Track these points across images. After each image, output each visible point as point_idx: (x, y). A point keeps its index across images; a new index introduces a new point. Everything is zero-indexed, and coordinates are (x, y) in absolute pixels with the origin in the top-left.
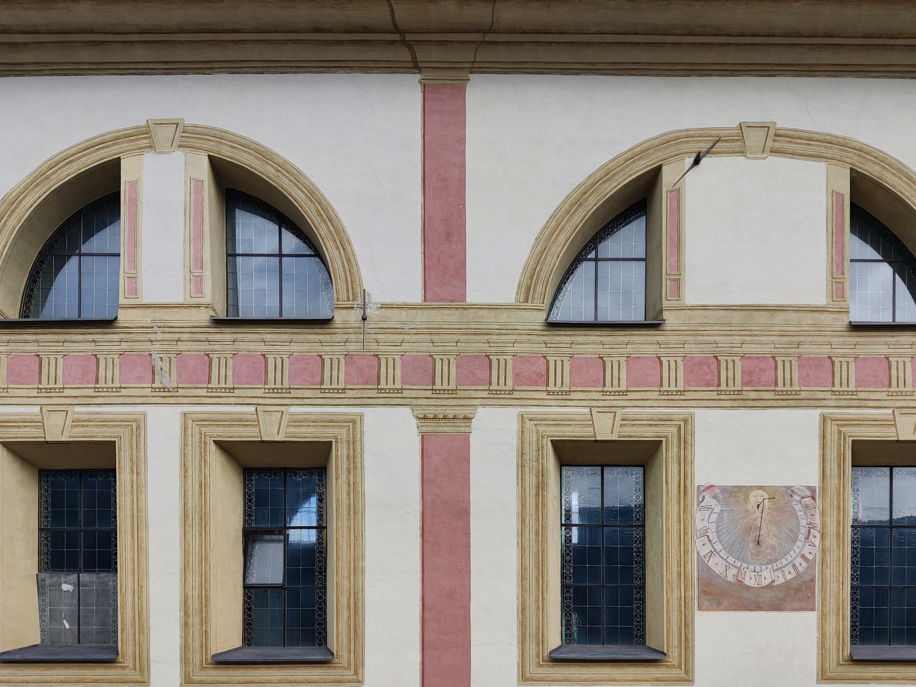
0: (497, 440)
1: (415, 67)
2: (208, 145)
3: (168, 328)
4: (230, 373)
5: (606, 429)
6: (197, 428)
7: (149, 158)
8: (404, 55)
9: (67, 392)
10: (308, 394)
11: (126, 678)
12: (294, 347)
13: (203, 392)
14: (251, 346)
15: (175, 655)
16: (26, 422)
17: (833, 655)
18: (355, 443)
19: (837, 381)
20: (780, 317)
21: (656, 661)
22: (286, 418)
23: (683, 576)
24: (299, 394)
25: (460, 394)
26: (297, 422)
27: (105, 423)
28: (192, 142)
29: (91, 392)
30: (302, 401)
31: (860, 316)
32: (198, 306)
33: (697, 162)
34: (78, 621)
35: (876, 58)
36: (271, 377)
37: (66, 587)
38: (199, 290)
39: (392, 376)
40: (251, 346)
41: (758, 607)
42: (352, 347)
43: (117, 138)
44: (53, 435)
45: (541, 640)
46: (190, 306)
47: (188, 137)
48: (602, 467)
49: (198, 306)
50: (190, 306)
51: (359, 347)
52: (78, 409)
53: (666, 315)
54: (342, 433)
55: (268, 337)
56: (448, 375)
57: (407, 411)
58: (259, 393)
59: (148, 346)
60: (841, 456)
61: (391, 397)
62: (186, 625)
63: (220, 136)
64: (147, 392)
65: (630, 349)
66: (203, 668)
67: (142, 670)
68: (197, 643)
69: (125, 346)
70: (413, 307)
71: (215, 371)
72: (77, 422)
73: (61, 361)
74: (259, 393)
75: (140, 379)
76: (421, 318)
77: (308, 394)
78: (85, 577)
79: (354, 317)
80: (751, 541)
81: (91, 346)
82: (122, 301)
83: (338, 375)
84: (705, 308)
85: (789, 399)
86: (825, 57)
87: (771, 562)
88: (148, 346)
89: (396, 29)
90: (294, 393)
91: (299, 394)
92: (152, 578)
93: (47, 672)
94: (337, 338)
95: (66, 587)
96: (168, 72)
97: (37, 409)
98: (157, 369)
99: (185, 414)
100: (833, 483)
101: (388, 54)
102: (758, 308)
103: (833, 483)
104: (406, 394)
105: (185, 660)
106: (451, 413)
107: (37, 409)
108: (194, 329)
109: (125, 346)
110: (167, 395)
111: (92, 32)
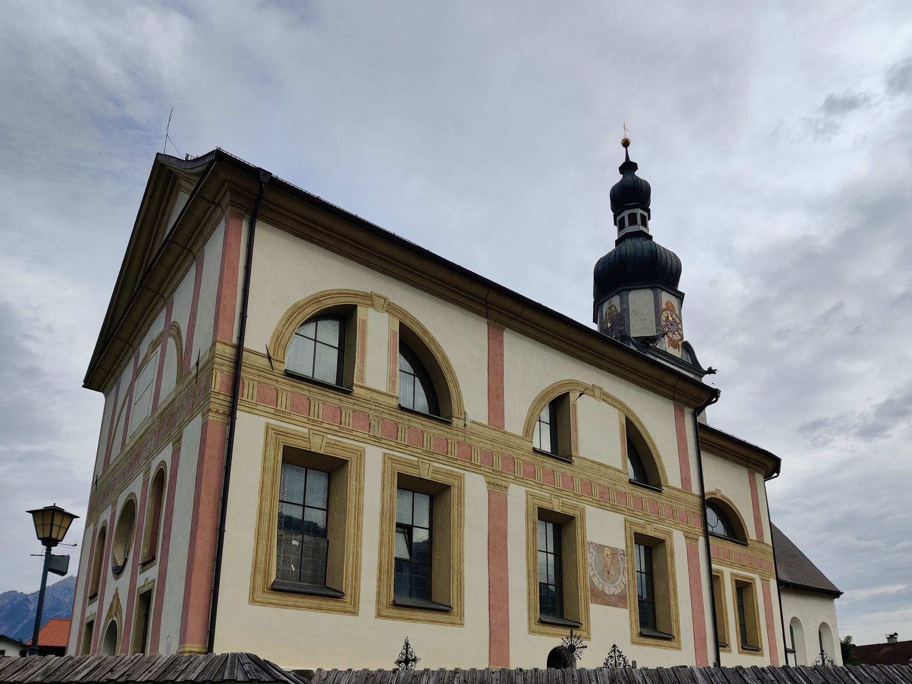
0: (518, 500)
1: (486, 316)
2: (400, 316)
3: (377, 403)
4: (289, 403)
5: (318, 445)
6: (390, 464)
7: (371, 311)
8: (484, 310)
9: (324, 425)
10: (441, 457)
11: (346, 609)
12: (435, 431)
13: (394, 444)
14: (416, 425)
15: (373, 598)
16: (299, 436)
17: (384, 601)
18: (461, 488)
19: (312, 413)
20: (609, 471)
21: (338, 597)
22: (431, 468)
23: (585, 585)
24: (437, 456)
25: (503, 474)
26: (436, 471)
27: (345, 448)
28: (392, 311)
29: (337, 429)
30: (438, 461)
31: (293, 368)
32: (392, 397)
33: (580, 395)
34: (300, 566)
35: (632, 376)
36: (425, 444)
37: (295, 542)
38: (394, 388)
39: (477, 459)
40: (416, 425)
41: (610, 605)
42: (461, 439)
43: (356, 294)
44: (557, 509)
45: (267, 573)
46: (389, 395)
47: (391, 309)
48: (414, 492)
49: (392, 397)
50: (389, 395)
51: (462, 439)
52: (329, 436)
53: (354, 388)
54: (456, 482)
55: (424, 423)
56: (499, 464)
57: (482, 477)
58: (420, 451)
59: (367, 410)
60: (631, 538)
61: (476, 469)
62: (379, 579)
63: (405, 314)
64: (366, 436)
65: (562, 470)
66: (388, 608)
67: (355, 605)
68: (385, 591)
69: (356, 407)
70: (483, 426)
71: (400, 434)
72: (329, 444)
73: (321, 406)
74: (420, 451)
75: (363, 428)
76: (488, 432)
77: (441, 457)
78: (307, 538)
79: (461, 423)
80: (606, 572)
81: (338, 402)
82: (355, 382)
83: (455, 452)
84: (586, 459)
85: (614, 509)
86: (618, 370)
87: (613, 583)
88: (367, 410)
89: (485, 301)
90: (435, 456)
91: (437, 456)
92: (465, 564)
93: (300, 600)
94: (454, 432)
95: (295, 542)
96: (383, 273)
97: (306, 431)
98: (372, 425)
99: (385, 454)
100: (630, 549)
101: (478, 307)
102: (602, 465)
103: (630, 549)
104: (482, 468)
105: (378, 602)
106: (500, 483)
107: (306, 431)
108: (390, 408)
109: (356, 407)
110: (377, 441)
111: (358, 243)
